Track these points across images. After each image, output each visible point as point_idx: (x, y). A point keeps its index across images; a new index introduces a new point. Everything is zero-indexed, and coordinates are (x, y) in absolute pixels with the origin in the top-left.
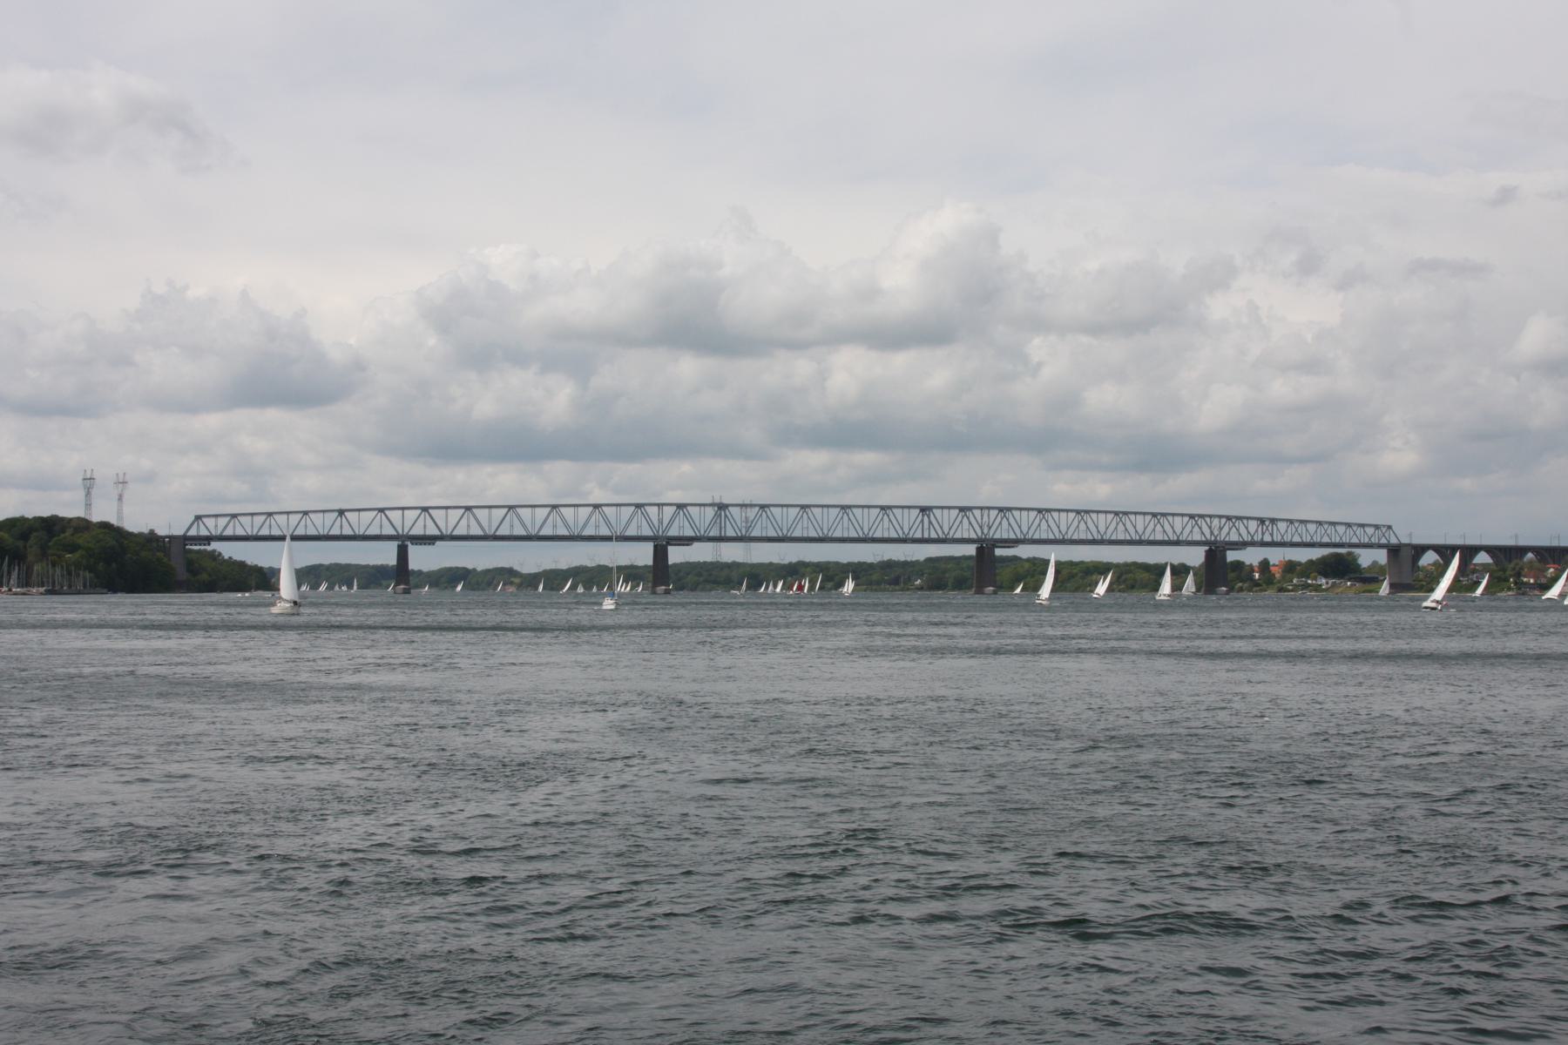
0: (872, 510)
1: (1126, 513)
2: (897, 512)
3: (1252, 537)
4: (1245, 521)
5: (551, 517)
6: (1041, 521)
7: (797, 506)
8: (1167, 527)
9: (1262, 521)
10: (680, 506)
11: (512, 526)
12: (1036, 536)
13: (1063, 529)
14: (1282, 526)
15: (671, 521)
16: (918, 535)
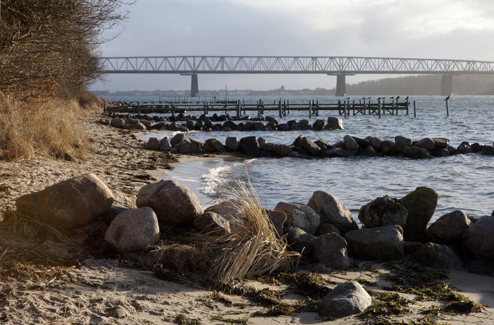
0: (380, 60)
1: (388, 59)
2: (301, 59)
3: (430, 70)
4: (461, 63)
5: (183, 63)
6: (367, 62)
7: (219, 57)
8: (407, 65)
9: (469, 62)
10: (203, 57)
11: (185, 67)
12: (365, 70)
13: (412, 67)
14: (478, 64)
15: (255, 64)
16: (311, 69)
